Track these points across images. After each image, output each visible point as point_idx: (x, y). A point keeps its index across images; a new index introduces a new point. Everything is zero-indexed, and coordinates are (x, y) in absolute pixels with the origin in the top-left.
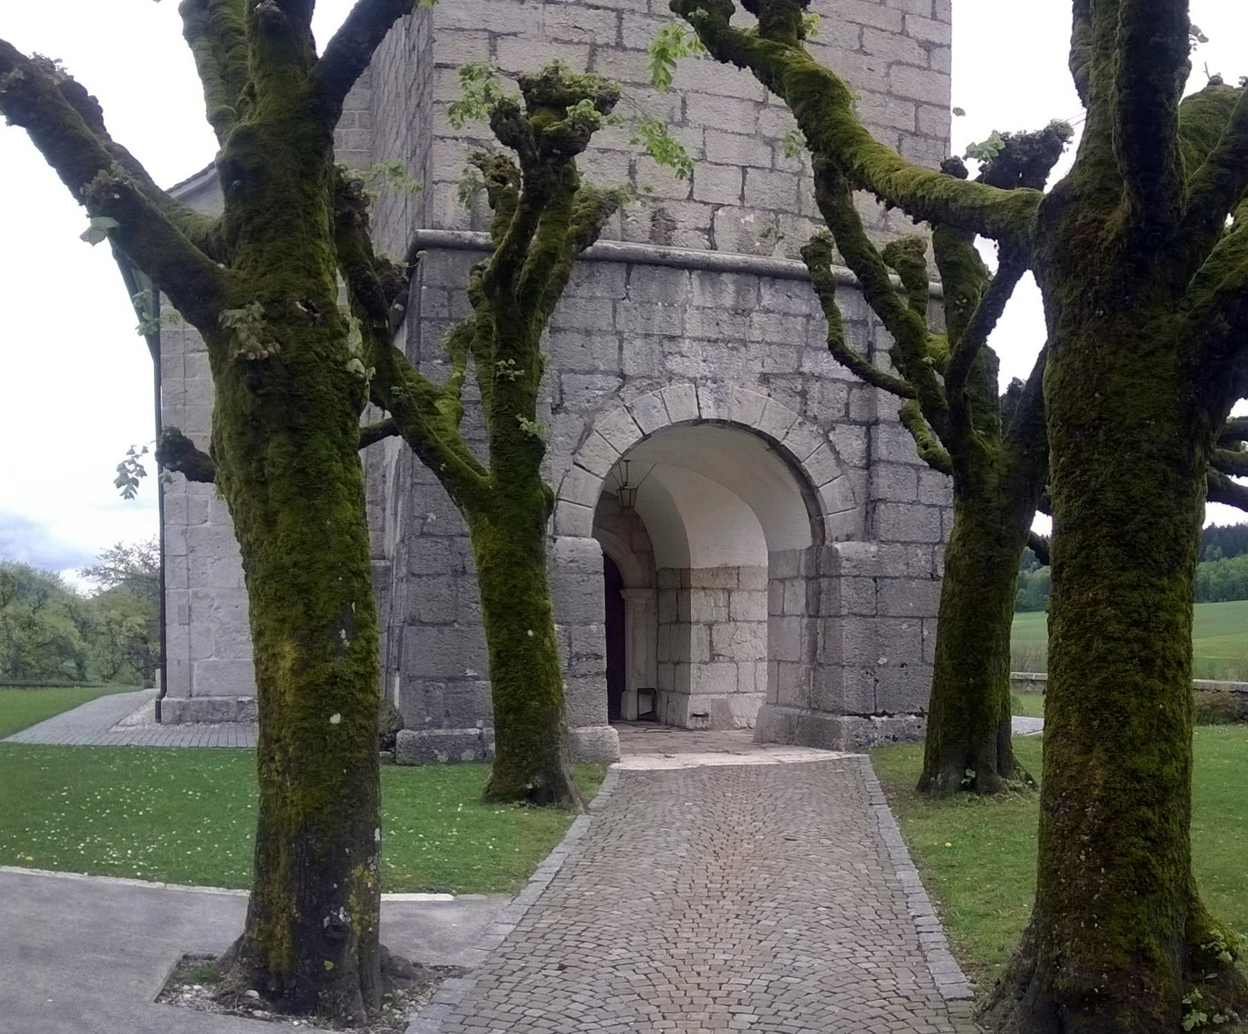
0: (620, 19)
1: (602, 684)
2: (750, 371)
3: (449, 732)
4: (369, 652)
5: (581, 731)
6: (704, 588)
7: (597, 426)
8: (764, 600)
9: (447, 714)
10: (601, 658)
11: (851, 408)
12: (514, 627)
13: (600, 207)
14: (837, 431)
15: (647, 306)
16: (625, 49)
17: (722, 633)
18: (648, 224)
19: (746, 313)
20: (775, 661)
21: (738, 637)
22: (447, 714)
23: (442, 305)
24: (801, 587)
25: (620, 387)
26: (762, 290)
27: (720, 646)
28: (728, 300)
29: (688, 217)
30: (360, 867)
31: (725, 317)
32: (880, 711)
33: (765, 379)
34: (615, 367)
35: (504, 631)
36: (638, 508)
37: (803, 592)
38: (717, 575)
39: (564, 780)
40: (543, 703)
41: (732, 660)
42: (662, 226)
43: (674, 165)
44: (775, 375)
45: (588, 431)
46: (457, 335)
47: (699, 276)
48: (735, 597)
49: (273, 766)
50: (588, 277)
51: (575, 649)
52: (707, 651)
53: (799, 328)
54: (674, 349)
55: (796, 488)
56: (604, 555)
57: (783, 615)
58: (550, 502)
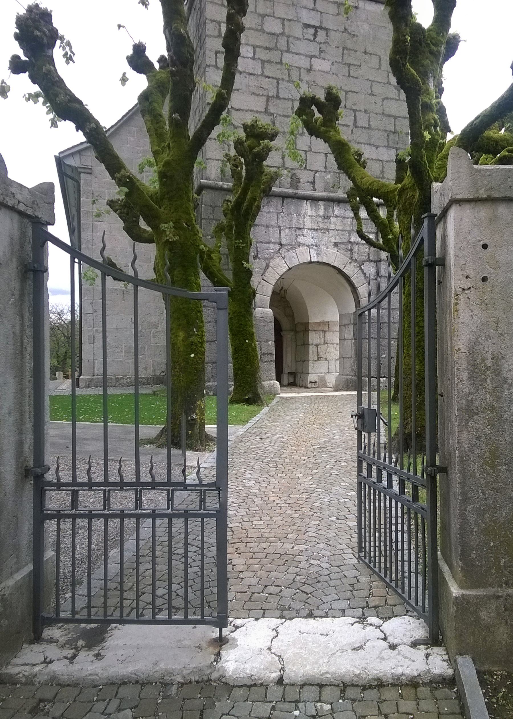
0: (278, 83)
1: (273, 365)
2: (330, 242)
3: (213, 383)
4: (202, 336)
5: (265, 383)
6: (314, 331)
7: (271, 264)
8: (338, 334)
9: (213, 377)
10: (273, 355)
11: (370, 255)
12: (241, 339)
13: (272, 178)
14: (365, 265)
15: (290, 215)
16: (280, 99)
17: (322, 348)
18: (289, 180)
19: (328, 217)
20: (342, 358)
21: (328, 350)
22: (213, 377)
23: (210, 213)
24: (351, 327)
25: (280, 249)
26: (335, 208)
27: (321, 354)
28: (321, 213)
29: (305, 176)
30: (200, 401)
31: (320, 219)
32: (383, 376)
33: (336, 245)
34: (278, 241)
35: (238, 340)
36: (288, 298)
37: (352, 330)
38: (320, 325)
39: (260, 395)
40: (252, 367)
41: (326, 359)
42: (295, 182)
43: (298, 162)
44: (340, 243)
45: (267, 266)
46: (217, 227)
47: (310, 202)
48: (327, 334)
49: (176, 370)
50: (267, 203)
51: (263, 352)
52: (316, 356)
53: (349, 223)
54: (301, 233)
55: (349, 289)
56: (275, 318)
57: (345, 339)
58: (254, 293)
